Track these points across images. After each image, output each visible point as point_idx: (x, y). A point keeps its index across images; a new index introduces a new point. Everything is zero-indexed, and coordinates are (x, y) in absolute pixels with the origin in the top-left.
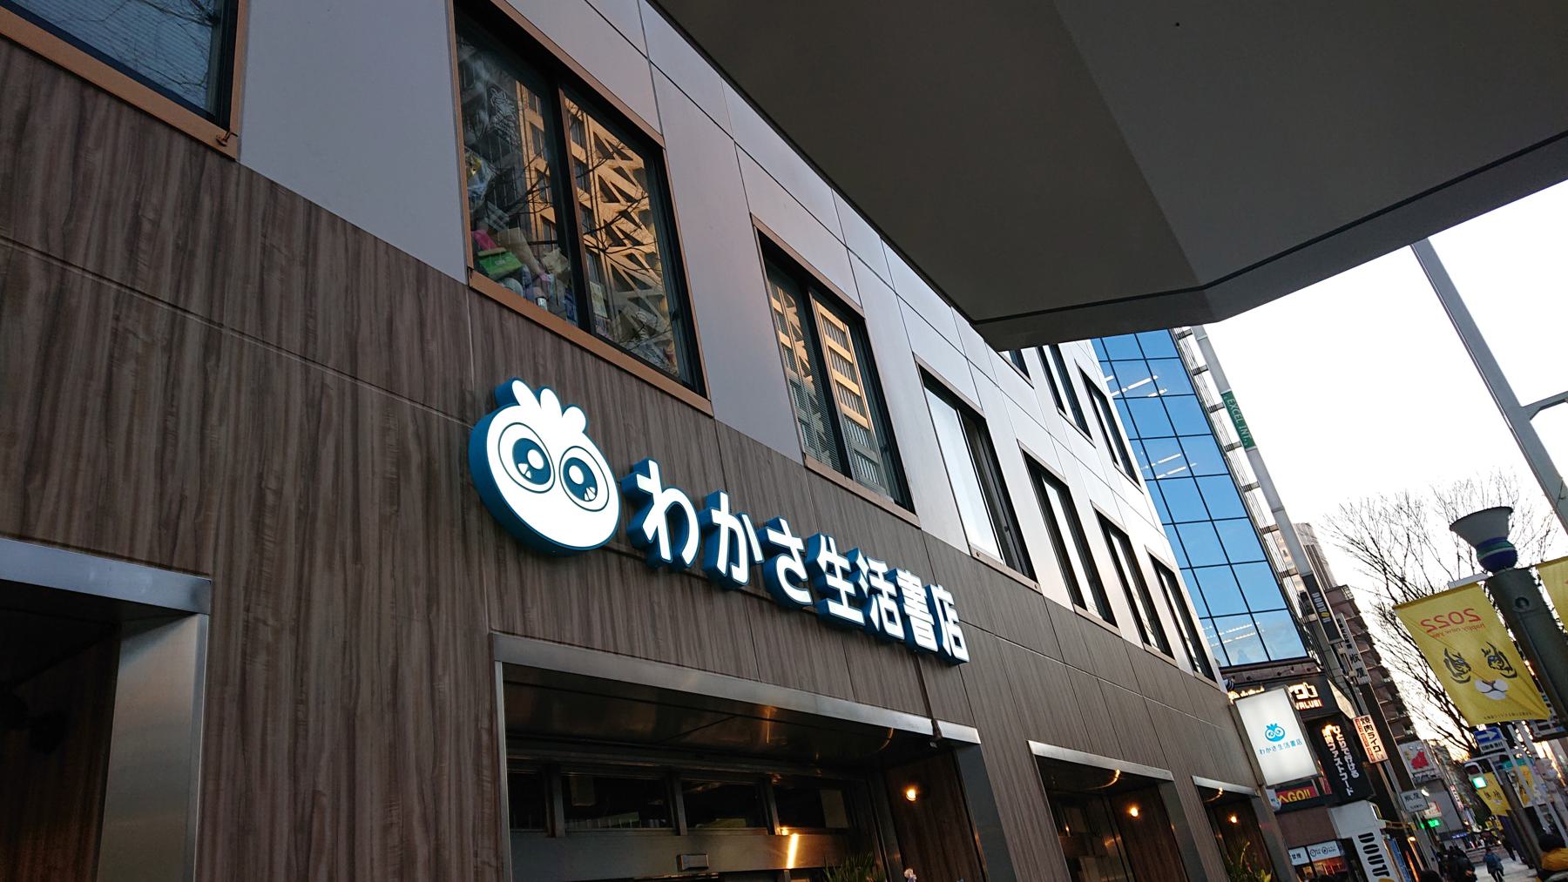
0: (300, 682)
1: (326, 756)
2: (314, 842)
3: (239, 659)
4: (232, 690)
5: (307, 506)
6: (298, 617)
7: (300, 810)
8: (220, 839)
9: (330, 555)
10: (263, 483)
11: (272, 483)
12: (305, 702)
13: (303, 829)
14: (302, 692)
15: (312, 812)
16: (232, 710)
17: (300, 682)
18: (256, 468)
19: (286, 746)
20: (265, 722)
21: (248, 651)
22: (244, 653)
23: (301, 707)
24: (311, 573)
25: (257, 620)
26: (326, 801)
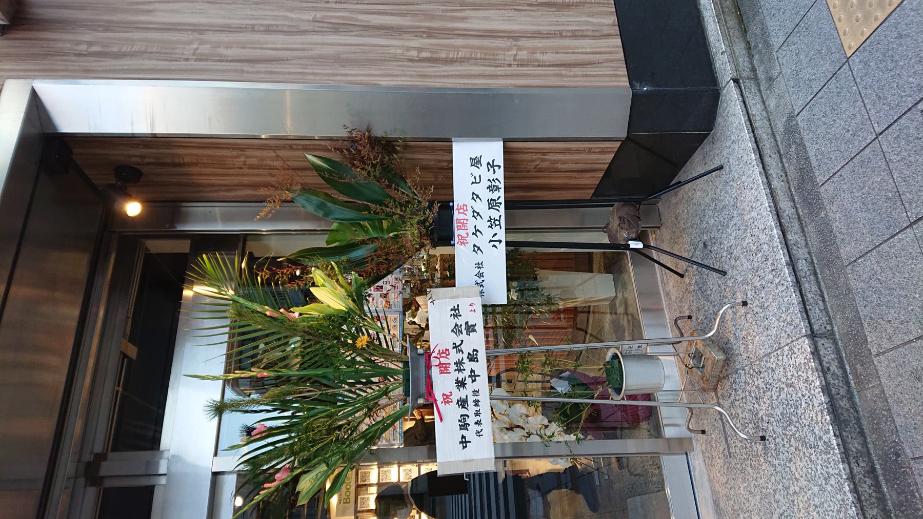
0: (549, 35)
1: (591, 20)
2: (345, 22)
3: (544, 68)
4: (246, 67)
5: (424, 32)
6: (190, 30)
7: (326, 29)
8: (342, 72)
9: (454, 19)
10: (416, 58)
11: (414, 53)
12: (253, 26)
13: (336, 28)
14: (246, 28)
15: (326, 22)
16: (262, 67)
17: (549, 35)
18: (405, 63)
19: (282, 37)
20: (577, 53)
21: (218, 58)
22: (220, 61)
23: (256, 28)
24: (155, 23)
25: (194, 54)
26: (319, 15)
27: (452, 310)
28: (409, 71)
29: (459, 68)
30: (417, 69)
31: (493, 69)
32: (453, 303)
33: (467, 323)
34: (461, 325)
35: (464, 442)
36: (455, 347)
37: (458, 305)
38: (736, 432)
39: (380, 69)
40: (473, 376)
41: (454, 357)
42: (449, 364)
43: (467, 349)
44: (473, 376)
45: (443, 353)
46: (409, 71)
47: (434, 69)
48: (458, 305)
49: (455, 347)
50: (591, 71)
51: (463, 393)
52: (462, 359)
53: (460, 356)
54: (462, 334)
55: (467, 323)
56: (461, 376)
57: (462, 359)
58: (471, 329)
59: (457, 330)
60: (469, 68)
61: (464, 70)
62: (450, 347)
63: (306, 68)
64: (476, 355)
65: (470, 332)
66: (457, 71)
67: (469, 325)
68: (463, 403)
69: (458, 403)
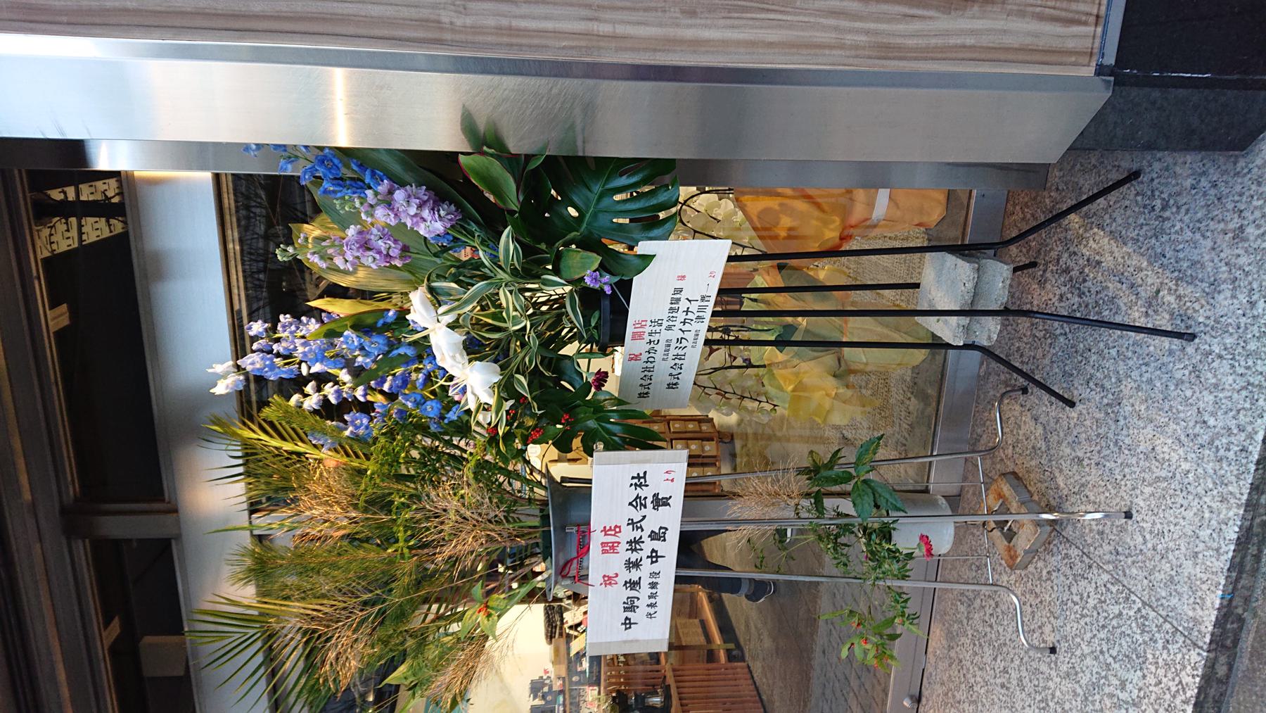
8: (689, 33)
27: (633, 478)
28: (851, 31)
29: (979, 24)
30: (872, 26)
31: (1058, 29)
32: (638, 469)
33: (656, 495)
34: (646, 498)
35: (628, 623)
36: (631, 523)
37: (645, 473)
38: (1021, 609)
39: (781, 25)
40: (654, 556)
41: (628, 534)
42: (619, 543)
43: (651, 525)
44: (654, 556)
45: (610, 529)
46: (851, 31)
47: (916, 26)
48: (645, 473)
49: (631, 523)
50: (523, 17)
51: (634, 575)
52: (641, 538)
53: (637, 534)
54: (645, 507)
55: (656, 495)
56: (634, 557)
57: (641, 538)
58: (659, 502)
59: (638, 503)
60: (1000, 24)
61: (990, 31)
62: (623, 524)
63: (596, 19)
64: (664, 533)
65: (659, 506)
66: (973, 32)
67: (660, 497)
68: (633, 585)
69: (625, 584)
